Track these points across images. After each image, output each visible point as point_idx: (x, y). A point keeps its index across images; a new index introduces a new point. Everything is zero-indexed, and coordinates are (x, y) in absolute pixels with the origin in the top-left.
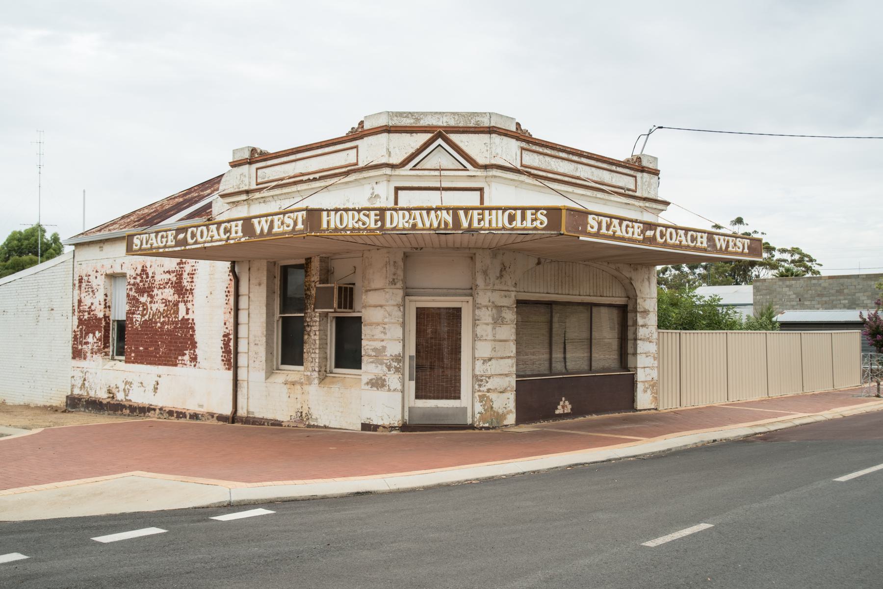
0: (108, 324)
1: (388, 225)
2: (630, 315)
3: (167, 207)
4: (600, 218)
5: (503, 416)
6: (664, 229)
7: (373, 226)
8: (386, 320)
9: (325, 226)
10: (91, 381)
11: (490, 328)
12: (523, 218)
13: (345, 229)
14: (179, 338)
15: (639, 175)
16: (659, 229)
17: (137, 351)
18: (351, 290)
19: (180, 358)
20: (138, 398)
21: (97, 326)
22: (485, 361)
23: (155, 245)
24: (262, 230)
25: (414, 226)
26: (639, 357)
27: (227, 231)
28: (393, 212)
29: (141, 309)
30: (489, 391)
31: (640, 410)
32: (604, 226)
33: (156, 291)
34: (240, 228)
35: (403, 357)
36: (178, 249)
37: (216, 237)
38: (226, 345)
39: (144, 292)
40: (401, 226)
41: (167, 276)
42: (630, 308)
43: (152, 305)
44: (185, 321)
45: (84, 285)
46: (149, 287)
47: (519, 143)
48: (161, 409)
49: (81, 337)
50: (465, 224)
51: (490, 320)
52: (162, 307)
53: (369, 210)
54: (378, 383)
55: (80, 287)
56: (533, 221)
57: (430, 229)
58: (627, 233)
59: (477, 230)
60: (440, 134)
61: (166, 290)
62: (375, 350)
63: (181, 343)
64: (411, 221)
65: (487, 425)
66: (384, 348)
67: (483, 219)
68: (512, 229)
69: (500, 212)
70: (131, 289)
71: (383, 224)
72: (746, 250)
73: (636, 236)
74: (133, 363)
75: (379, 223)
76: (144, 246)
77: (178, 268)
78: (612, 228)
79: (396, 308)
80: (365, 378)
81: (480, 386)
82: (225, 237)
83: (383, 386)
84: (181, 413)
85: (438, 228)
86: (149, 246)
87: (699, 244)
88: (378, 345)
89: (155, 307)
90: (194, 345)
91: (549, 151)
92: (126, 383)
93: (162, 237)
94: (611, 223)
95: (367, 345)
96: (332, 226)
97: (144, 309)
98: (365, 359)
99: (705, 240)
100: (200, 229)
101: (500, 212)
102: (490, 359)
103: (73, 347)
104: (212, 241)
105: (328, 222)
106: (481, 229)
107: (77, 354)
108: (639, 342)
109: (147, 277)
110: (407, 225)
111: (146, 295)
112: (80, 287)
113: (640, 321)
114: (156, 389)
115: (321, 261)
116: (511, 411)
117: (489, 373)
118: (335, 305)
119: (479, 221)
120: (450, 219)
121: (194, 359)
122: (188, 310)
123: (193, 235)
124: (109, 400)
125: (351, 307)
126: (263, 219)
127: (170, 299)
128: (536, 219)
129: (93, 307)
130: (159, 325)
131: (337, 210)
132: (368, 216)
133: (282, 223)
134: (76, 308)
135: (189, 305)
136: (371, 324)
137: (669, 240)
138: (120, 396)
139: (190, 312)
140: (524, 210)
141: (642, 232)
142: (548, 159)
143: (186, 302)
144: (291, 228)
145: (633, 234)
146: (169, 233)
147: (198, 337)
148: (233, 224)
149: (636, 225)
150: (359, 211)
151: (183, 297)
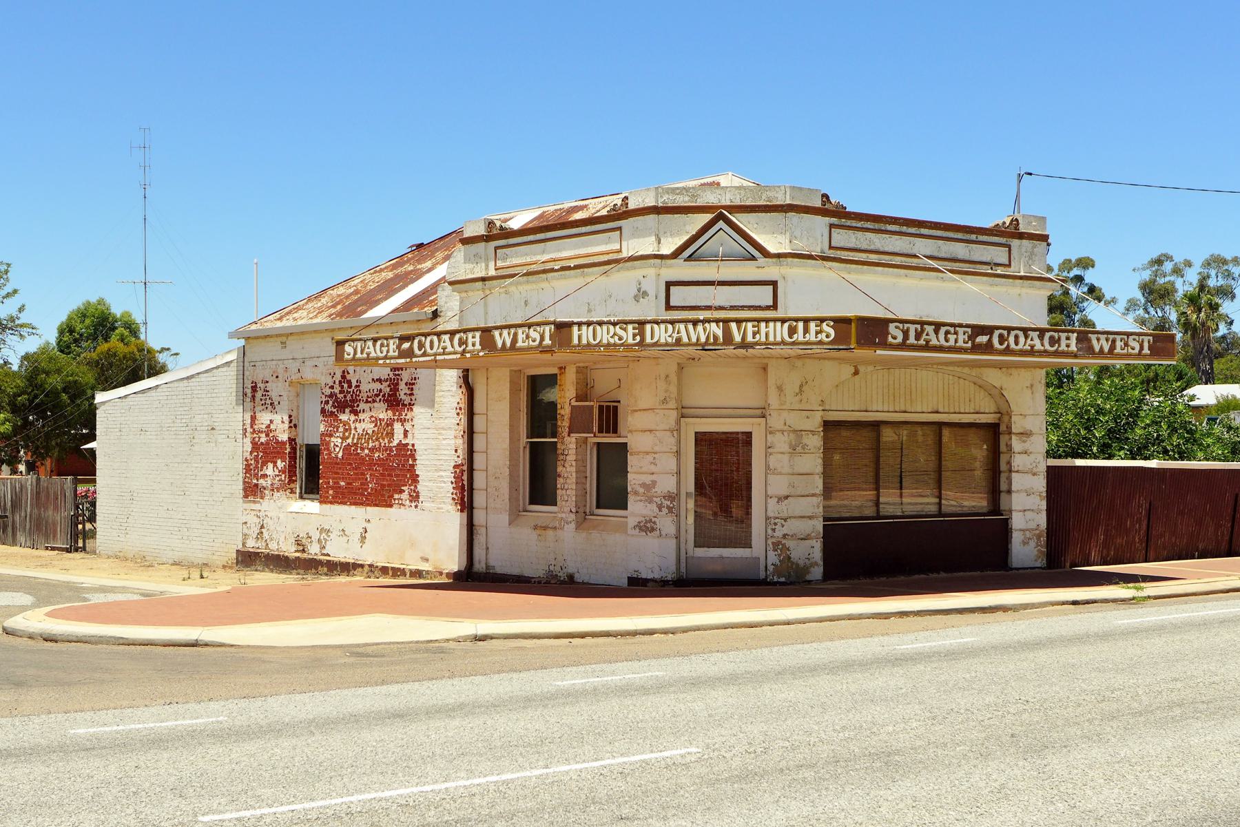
0: (294, 449)
1: (648, 340)
2: (1003, 439)
3: (372, 286)
4: (906, 326)
5: (806, 569)
6: (1005, 333)
7: (630, 341)
8: (657, 449)
9: (575, 341)
10: (272, 528)
11: (786, 457)
12: (806, 330)
13: (598, 345)
14: (393, 469)
15: (1015, 243)
16: (997, 333)
17: (336, 488)
18: (616, 408)
19: (396, 496)
20: (338, 551)
21: (278, 453)
22: (781, 499)
23: (373, 355)
24: (504, 343)
25: (679, 340)
26: (1014, 495)
27: (461, 343)
28: (655, 326)
29: (341, 429)
30: (785, 536)
31: (1018, 569)
32: (912, 334)
33: (362, 406)
34: (477, 340)
35: (678, 494)
36: (403, 361)
37: (449, 349)
38: (458, 478)
39: (346, 407)
40: (663, 341)
41: (377, 386)
42: (1003, 428)
43: (358, 425)
44: (402, 447)
45: (259, 395)
46: (353, 401)
47: (828, 220)
48: (371, 566)
49: (256, 467)
50: (738, 338)
51: (786, 448)
52: (370, 427)
53: (626, 323)
54: (647, 527)
55: (253, 397)
56: (817, 333)
57: (696, 344)
58: (947, 340)
59: (751, 346)
60: (720, 215)
61: (376, 404)
62: (643, 485)
63: (397, 476)
64: (675, 335)
65: (783, 580)
66: (654, 483)
67: (758, 332)
68: (793, 343)
69: (779, 324)
70: (327, 402)
71: (643, 339)
72: (1146, 351)
73: (960, 343)
74: (331, 503)
75: (638, 338)
76: (359, 355)
77: (392, 376)
78: (924, 336)
79: (668, 433)
80: (632, 521)
81: (774, 530)
82: (460, 349)
83: (653, 530)
84: (399, 569)
85: (706, 343)
86: (365, 355)
87: (1063, 347)
88: (647, 479)
89: (360, 427)
90: (415, 479)
91: (869, 225)
92: (322, 530)
93: (382, 345)
94: (923, 330)
95: (634, 479)
96: (584, 341)
97: (346, 430)
98: (631, 499)
99: (1073, 342)
100: (429, 339)
101: (779, 324)
102: (787, 497)
103: (244, 482)
104: (444, 354)
105: (580, 337)
106: (757, 344)
107: (252, 491)
108: (1014, 475)
109: (350, 386)
110: (670, 340)
111: (347, 410)
112: (253, 397)
113: (1016, 444)
114: (363, 539)
115: (577, 372)
116: (816, 564)
117: (785, 515)
118: (595, 429)
119: (754, 334)
120: (720, 333)
121: (415, 497)
122: (406, 433)
123: (421, 346)
124: (298, 554)
125: (615, 431)
126: (505, 332)
127: (381, 416)
128: (821, 332)
129: (272, 427)
130: (367, 451)
131: (589, 324)
132: (625, 330)
133: (528, 337)
134: (248, 427)
135: (408, 426)
136: (638, 453)
137: (1013, 346)
138: (314, 550)
139: (410, 435)
140: (806, 321)
141: (970, 338)
142: (869, 235)
143: (403, 421)
144: (537, 343)
145: (956, 341)
146: (391, 342)
147: (419, 470)
148: (470, 335)
149: (960, 330)
150: (615, 324)
151: (400, 414)
